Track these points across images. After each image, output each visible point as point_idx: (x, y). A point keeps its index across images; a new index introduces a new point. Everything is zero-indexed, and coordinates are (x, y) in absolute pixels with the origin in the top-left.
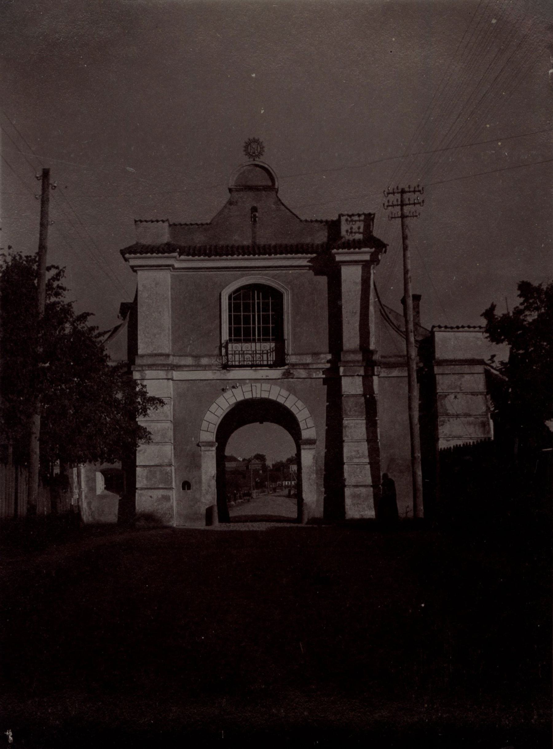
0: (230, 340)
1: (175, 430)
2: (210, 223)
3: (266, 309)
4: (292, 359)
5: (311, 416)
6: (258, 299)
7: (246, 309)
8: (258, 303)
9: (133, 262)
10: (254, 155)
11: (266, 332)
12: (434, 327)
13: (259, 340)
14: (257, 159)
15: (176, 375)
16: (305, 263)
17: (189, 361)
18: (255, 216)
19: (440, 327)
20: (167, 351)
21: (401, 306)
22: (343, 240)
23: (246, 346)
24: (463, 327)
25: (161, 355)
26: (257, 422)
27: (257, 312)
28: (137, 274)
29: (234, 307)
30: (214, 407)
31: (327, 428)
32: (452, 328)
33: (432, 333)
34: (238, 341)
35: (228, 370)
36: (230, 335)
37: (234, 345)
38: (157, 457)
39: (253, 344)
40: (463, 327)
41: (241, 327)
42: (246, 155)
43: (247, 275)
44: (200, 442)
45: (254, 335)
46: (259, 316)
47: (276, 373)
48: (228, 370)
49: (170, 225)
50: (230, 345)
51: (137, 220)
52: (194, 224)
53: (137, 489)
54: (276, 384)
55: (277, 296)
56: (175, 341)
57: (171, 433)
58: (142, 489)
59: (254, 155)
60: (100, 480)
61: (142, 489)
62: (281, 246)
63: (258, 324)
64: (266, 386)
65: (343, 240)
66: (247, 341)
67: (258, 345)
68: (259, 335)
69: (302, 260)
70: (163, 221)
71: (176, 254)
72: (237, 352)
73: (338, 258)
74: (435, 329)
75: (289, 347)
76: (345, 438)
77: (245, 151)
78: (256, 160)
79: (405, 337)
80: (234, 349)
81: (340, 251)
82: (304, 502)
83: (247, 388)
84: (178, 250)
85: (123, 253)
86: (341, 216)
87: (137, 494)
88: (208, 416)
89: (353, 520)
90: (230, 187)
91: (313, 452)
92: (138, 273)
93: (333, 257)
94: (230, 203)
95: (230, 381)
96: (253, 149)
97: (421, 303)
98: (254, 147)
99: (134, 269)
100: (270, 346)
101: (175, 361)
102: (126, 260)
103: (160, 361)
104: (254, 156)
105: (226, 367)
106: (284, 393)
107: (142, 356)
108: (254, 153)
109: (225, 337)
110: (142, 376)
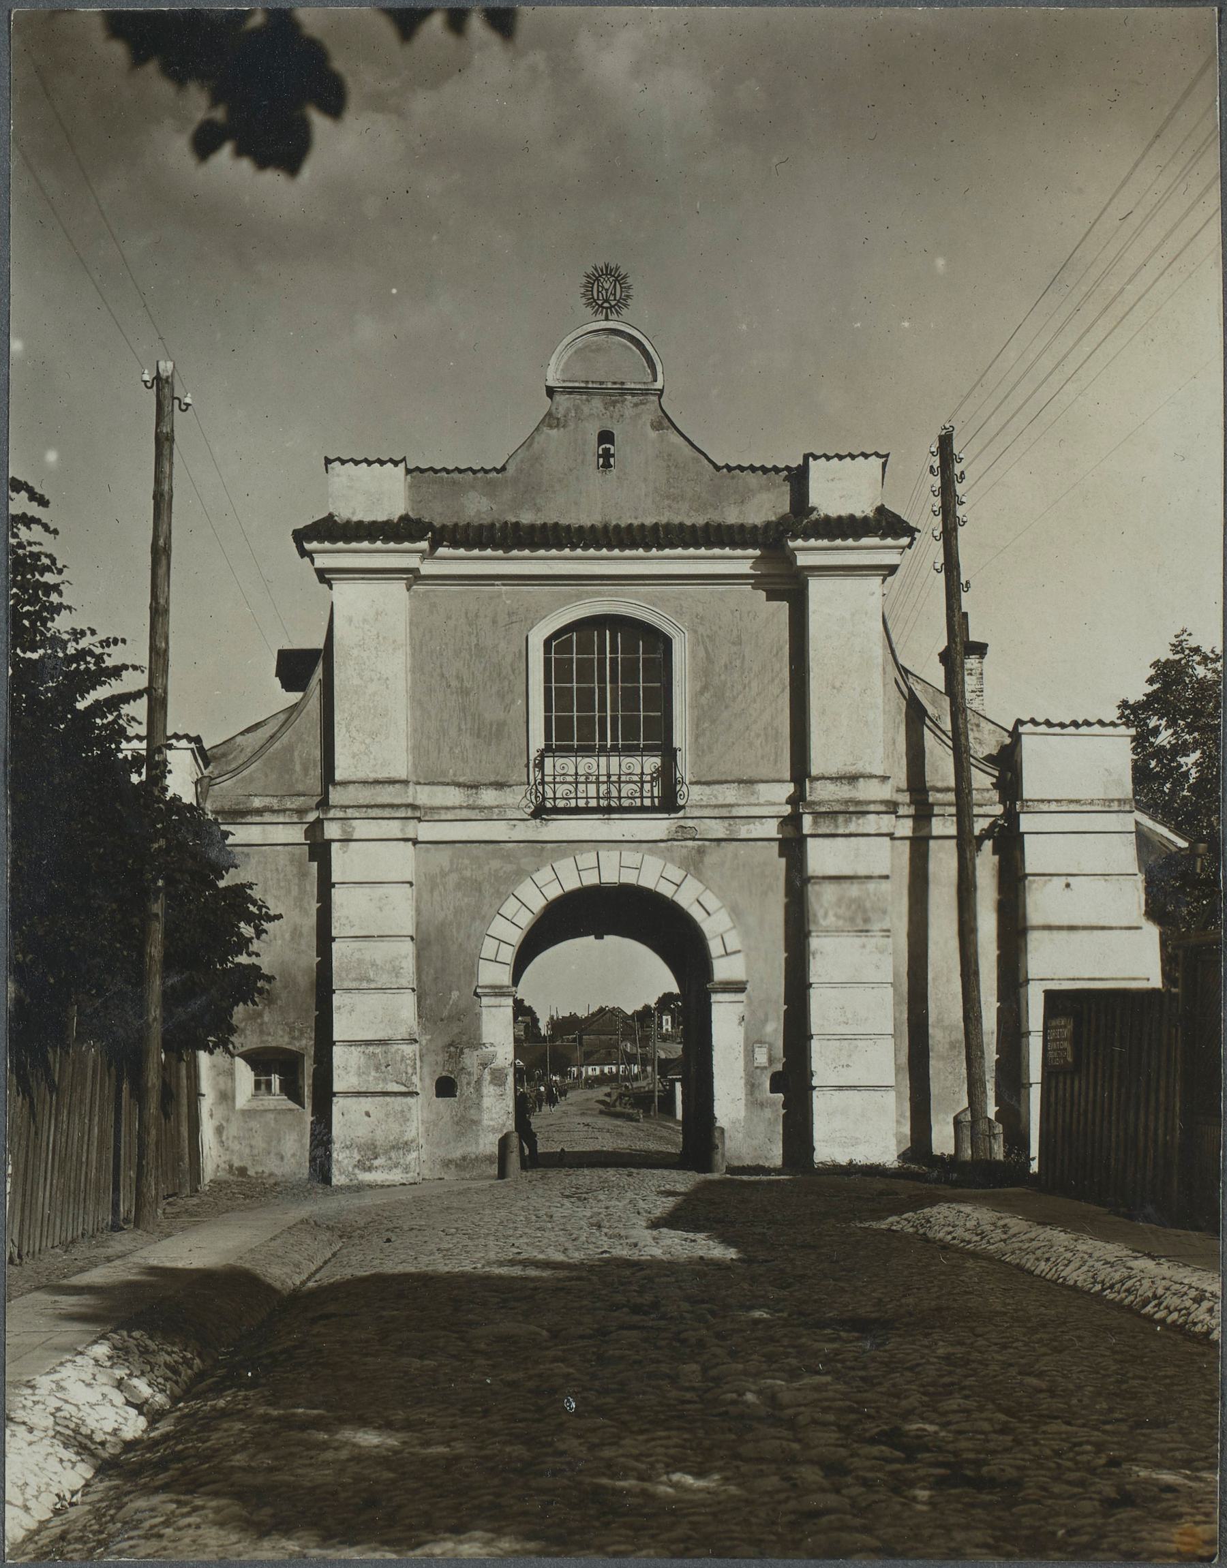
0: (548, 750)
1: (419, 957)
2: (504, 468)
3: (630, 673)
4: (692, 795)
5: (734, 927)
6: (614, 650)
7: (584, 675)
8: (614, 661)
9: (322, 561)
10: (606, 305)
11: (631, 730)
12: (1020, 722)
13: (614, 748)
14: (615, 316)
15: (426, 831)
16: (745, 568)
17: (453, 796)
18: (607, 451)
19: (1033, 722)
20: (401, 772)
21: (941, 670)
22: (814, 516)
23: (586, 764)
24: (1087, 723)
25: (392, 782)
26: (588, 934)
27: (610, 683)
28: (331, 588)
29: (555, 670)
30: (510, 907)
31: (999, 1004)
32: (1062, 725)
33: (1015, 735)
34: (566, 750)
35: (545, 820)
36: (548, 736)
37: (560, 761)
38: (382, 1022)
39: (603, 760)
40: (1087, 723)
41: (572, 717)
42: (588, 305)
43: (589, 594)
44: (478, 986)
45: (603, 737)
46: (614, 691)
47: (657, 827)
48: (545, 820)
49: (408, 471)
50: (548, 762)
51: (332, 458)
52: (490, 471)
53: (334, 1094)
54: (652, 852)
55: (659, 642)
56: (417, 750)
57: (409, 965)
58: (346, 1094)
59: (606, 305)
60: (245, 1075)
61: (346, 1094)
62: (668, 527)
63: (612, 710)
64: (631, 857)
65: (814, 516)
66: (586, 750)
67: (614, 761)
68: (614, 738)
69: (741, 562)
70: (396, 463)
71: (424, 545)
72: (593, 779)
73: (802, 560)
74: (1021, 729)
75: (685, 767)
76: (812, 979)
77: (584, 295)
78: (610, 318)
79: (950, 743)
80: (559, 770)
81: (812, 542)
82: (718, 1124)
83: (587, 859)
84: (430, 534)
85: (300, 536)
86: (811, 459)
87: (335, 1109)
88: (499, 927)
89: (835, 1170)
90: (551, 383)
91: (740, 1009)
92: (334, 586)
93: (790, 558)
94: (550, 420)
95: (549, 845)
96: (604, 292)
97: (32, 540)
98: (606, 286)
99: (323, 576)
100: (652, 763)
101: (419, 796)
102: (304, 553)
103: (387, 795)
104: (607, 308)
105: (541, 812)
106: (675, 873)
107: (344, 784)
108: (607, 301)
109: (538, 741)
110: (344, 831)
